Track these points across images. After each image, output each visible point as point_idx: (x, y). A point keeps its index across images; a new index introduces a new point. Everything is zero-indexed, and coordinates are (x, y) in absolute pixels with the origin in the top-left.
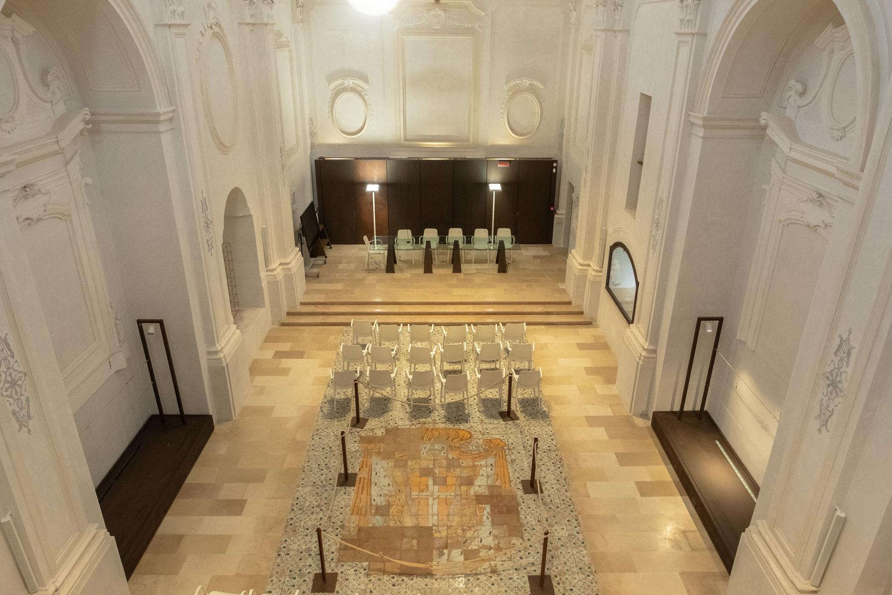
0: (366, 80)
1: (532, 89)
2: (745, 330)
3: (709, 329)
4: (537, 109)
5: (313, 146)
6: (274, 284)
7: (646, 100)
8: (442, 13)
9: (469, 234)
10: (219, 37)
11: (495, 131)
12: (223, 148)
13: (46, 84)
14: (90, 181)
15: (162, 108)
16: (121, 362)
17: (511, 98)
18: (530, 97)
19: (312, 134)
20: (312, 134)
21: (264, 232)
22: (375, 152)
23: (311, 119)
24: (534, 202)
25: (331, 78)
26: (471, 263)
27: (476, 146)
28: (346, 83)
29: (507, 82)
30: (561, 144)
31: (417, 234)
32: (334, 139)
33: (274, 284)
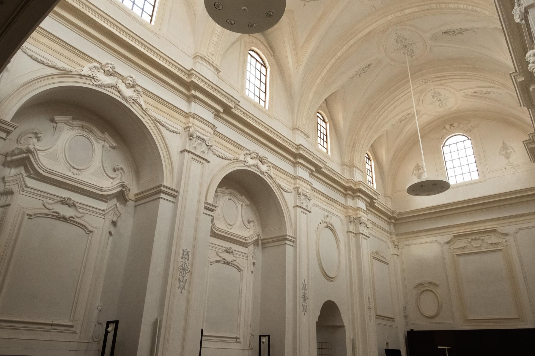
3: (264, 340)
21: (353, 341)
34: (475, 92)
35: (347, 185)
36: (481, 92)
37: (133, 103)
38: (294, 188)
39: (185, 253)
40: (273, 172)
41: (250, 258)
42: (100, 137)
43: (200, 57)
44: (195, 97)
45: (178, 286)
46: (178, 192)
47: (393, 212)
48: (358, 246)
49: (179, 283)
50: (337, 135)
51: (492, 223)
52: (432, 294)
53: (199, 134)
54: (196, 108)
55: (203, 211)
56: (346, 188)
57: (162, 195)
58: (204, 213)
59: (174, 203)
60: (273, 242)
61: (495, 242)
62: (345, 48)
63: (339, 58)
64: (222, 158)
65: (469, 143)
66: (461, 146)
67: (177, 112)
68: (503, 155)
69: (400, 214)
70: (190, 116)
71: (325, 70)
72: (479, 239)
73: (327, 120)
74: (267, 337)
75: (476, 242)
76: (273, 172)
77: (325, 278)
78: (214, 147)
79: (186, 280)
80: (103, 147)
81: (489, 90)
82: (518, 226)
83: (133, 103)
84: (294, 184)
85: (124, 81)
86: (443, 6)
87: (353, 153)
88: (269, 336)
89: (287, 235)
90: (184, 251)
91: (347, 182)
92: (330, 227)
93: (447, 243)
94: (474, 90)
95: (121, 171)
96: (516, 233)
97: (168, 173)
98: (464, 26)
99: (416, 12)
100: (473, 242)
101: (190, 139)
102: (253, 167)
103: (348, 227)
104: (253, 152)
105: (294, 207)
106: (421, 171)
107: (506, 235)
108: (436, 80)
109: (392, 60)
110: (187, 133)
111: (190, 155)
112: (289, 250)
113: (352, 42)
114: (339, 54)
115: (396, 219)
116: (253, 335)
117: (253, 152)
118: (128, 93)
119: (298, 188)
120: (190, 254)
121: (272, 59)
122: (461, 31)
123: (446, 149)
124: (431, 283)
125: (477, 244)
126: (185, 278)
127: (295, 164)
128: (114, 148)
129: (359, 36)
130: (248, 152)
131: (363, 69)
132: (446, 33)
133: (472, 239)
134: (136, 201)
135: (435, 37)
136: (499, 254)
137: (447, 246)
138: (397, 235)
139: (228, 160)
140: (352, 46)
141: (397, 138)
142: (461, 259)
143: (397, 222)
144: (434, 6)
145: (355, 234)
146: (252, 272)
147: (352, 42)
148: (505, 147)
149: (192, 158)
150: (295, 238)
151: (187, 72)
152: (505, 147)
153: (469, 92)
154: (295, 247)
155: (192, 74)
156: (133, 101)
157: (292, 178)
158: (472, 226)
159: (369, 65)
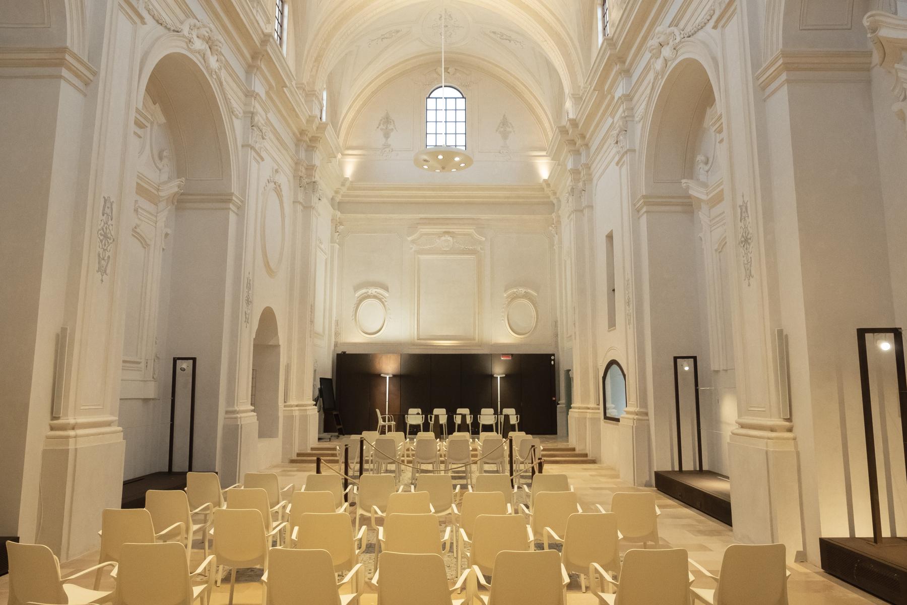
0: (386, 289)
1: (526, 296)
2: (714, 361)
3: (686, 367)
4: (534, 313)
5: (336, 345)
6: (290, 419)
7: (610, 237)
8: (450, 239)
9: (475, 413)
10: (278, 190)
11: (499, 332)
12: (270, 272)
13: (161, 158)
14: (169, 231)
15: (235, 189)
16: (151, 391)
17: (509, 303)
18: (525, 301)
19: (337, 334)
20: (337, 334)
21: (288, 368)
22: (389, 348)
23: (337, 322)
24: (535, 391)
25: (357, 288)
26: (450, 62)
27: (480, 345)
28: (370, 292)
29: (506, 290)
30: (557, 342)
31: (427, 411)
32: (355, 338)
33: (290, 419)
34: (494, 33)
38: (244, 113)
39: (108, 205)
40: (224, 74)
49: (99, 263)
55: (132, 127)
57: (65, 72)
58: (135, 133)
59: (85, 95)
64: (157, 21)
65: (461, 103)
66: (451, 104)
70: (252, 96)
74: (191, 361)
76: (224, 74)
79: (109, 257)
88: (194, 359)
89: (232, 194)
90: (105, 201)
97: (75, 25)
102: (198, 55)
106: (391, 127)
112: (68, 97)
116: (158, 358)
117: (204, 26)
119: (253, 113)
120: (114, 206)
123: (431, 103)
126: (107, 254)
130: (198, 24)
145: (304, 207)
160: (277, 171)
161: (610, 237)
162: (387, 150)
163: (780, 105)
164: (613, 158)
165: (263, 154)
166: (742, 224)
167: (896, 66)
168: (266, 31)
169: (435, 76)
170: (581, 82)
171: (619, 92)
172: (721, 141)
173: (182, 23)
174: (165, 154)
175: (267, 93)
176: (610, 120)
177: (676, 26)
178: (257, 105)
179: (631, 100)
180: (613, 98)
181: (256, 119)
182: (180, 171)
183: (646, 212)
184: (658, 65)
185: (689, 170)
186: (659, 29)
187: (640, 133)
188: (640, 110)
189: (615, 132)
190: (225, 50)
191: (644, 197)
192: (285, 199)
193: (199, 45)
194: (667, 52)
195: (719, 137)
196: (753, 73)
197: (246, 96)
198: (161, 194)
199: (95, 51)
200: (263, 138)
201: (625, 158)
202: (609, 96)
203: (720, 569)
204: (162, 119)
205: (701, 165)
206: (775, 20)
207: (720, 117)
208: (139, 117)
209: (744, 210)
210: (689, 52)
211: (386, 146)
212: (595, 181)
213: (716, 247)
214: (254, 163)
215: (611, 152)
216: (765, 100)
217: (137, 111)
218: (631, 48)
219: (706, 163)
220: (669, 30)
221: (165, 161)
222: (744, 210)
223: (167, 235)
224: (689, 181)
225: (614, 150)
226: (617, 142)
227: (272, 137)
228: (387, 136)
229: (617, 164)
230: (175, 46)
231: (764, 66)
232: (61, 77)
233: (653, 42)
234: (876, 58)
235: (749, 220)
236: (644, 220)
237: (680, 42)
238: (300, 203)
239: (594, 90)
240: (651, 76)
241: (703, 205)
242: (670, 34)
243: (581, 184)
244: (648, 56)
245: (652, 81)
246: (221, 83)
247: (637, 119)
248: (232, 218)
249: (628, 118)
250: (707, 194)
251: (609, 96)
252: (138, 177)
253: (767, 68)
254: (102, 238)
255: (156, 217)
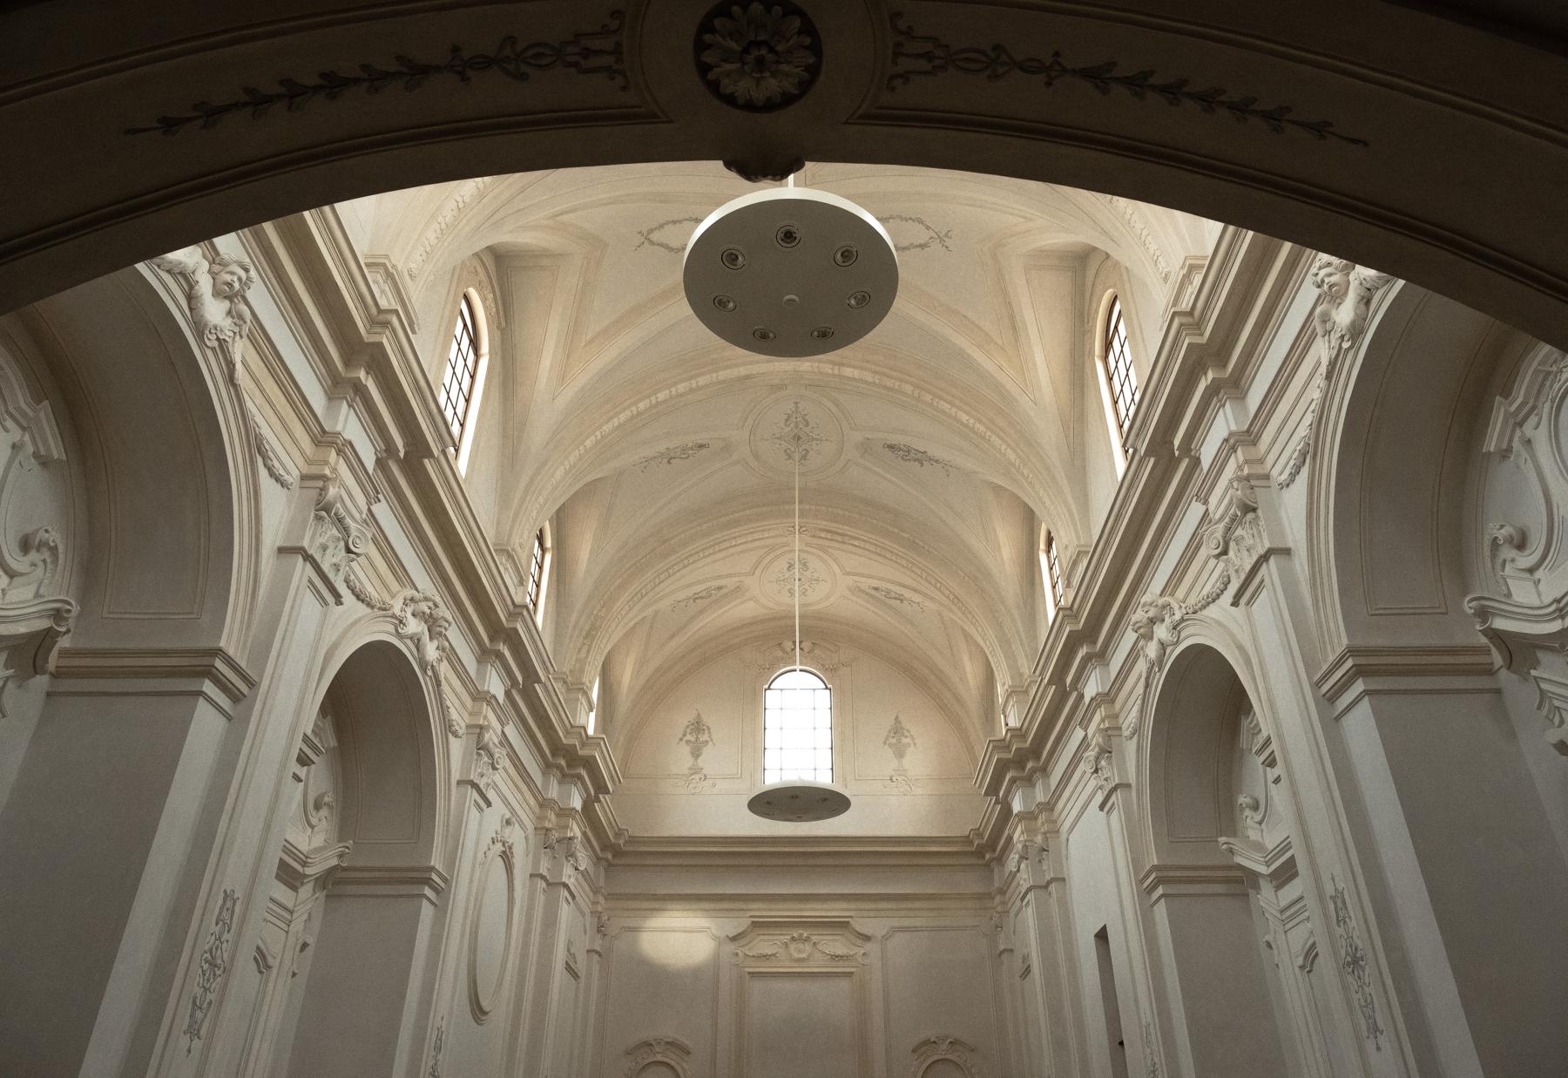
10: (507, 857)
13: (317, 807)
14: (311, 940)
34: (876, 589)
35: (565, 741)
36: (888, 592)
37: (213, 349)
38: (468, 727)
39: (229, 904)
40: (240, 350)
41: (298, 925)
42: (19, 409)
43: (386, 270)
44: (359, 389)
45: (185, 1027)
46: (251, 684)
47: (618, 834)
48: (550, 921)
49: (192, 1016)
50: (558, 591)
51: (844, 905)
52: (663, 1069)
53: (342, 512)
54: (350, 425)
56: (557, 748)
57: (208, 687)
59: (229, 718)
60: (377, 882)
61: (839, 952)
62: (682, 388)
63: (658, 404)
65: (824, 697)
67: (1129, 671)
68: (891, 746)
69: (633, 840)
70: (332, 444)
71: (616, 422)
72: (808, 939)
73: (548, 543)
75: (801, 946)
76: (444, 669)
77: (472, 1011)
78: (362, 559)
80: (14, 446)
81: (907, 594)
82: (895, 923)
83: (213, 349)
84: (471, 714)
85: (216, 268)
86: (928, 398)
87: (584, 650)
91: (567, 733)
92: (507, 857)
93: (734, 939)
94: (876, 583)
95: (46, 555)
96: (886, 938)
98: (935, 451)
99: (866, 382)
100: (792, 947)
101: (319, 518)
102: (409, 642)
103: (536, 863)
104: (426, 599)
105: (459, 783)
106: (705, 737)
107: (867, 938)
108: (823, 535)
109: (756, 457)
110: (314, 494)
111: (309, 569)
112: (206, 725)
113: (702, 381)
114: (661, 396)
115: (618, 853)
117: (426, 599)
118: (215, 311)
119: (481, 727)
121: (498, 333)
122: (922, 458)
124: (672, 1044)
125: (800, 951)
126: (210, 996)
127: (337, 386)
128: (44, 462)
129: (723, 375)
131: (684, 449)
132: (891, 447)
133: (793, 939)
134: (56, 675)
135: (865, 447)
136: (844, 984)
137: (731, 947)
138: (610, 897)
139: (368, 605)
140: (699, 388)
141: (673, 636)
142: (757, 986)
143: (618, 861)
144: (908, 388)
145: (549, 884)
146: (294, 974)
147: (702, 381)
148: (897, 730)
149: (310, 581)
150: (445, 880)
151: (374, 311)
152: (897, 730)
153: (866, 583)
154: (441, 910)
155: (386, 324)
156: (216, 344)
157: (471, 694)
158: (819, 906)
159: (701, 446)
160: (508, 822)
161: (1102, 936)
162: (697, 777)
163: (1361, 726)
164: (1093, 794)
165: (491, 795)
166: (1340, 931)
167: (1533, 672)
168: (517, 600)
169: (780, 654)
170: (1026, 668)
171: (1091, 689)
172: (1277, 780)
173: (393, 597)
174: (326, 799)
175: (508, 694)
176: (1079, 734)
177: (1172, 594)
178: (491, 715)
179: (1113, 701)
180: (1081, 696)
181: (487, 736)
182: (346, 826)
183: (1366, 692)
184: (1152, 650)
185: (1226, 815)
186: (1146, 598)
187: (1133, 759)
188: (1130, 719)
189: (1091, 754)
190: (455, 636)
191: (1155, 868)
192: (517, 871)
193: (414, 626)
194: (1161, 632)
195: (1272, 773)
196: (1310, 677)
197: (474, 699)
198: (308, 871)
199: (262, 650)
200: (494, 768)
201: (1113, 798)
202: (1075, 694)
203: (233, 235)
204: (333, 743)
205: (1247, 812)
206: (1328, 600)
207: (1268, 741)
208: (306, 749)
209: (1340, 905)
210: (1195, 636)
211: (695, 770)
212: (1064, 836)
213: (1300, 961)
214: (474, 810)
215: (1087, 786)
216: (1338, 718)
217: (306, 739)
218: (1104, 620)
219: (1256, 808)
220: (1161, 601)
221: (324, 812)
222: (1340, 905)
223: (305, 946)
224: (1231, 840)
225: (1093, 783)
226: (1096, 771)
227: (507, 763)
228: (696, 754)
229: (1102, 807)
230: (381, 632)
231: (1325, 667)
232: (200, 693)
233: (1139, 616)
234: (1497, 659)
235: (1353, 923)
236: (1161, 911)
237: (1182, 620)
238: (543, 877)
239: (1050, 683)
240: (1141, 667)
241: (1262, 882)
242: (1164, 607)
243: (1039, 839)
244: (1129, 638)
245: (1144, 675)
246: (439, 684)
247: (1127, 733)
248: (427, 911)
249: (1111, 731)
250: (1268, 864)
251: (1075, 694)
252: (286, 850)
253: (1330, 672)
254: (206, 966)
255: (291, 912)
